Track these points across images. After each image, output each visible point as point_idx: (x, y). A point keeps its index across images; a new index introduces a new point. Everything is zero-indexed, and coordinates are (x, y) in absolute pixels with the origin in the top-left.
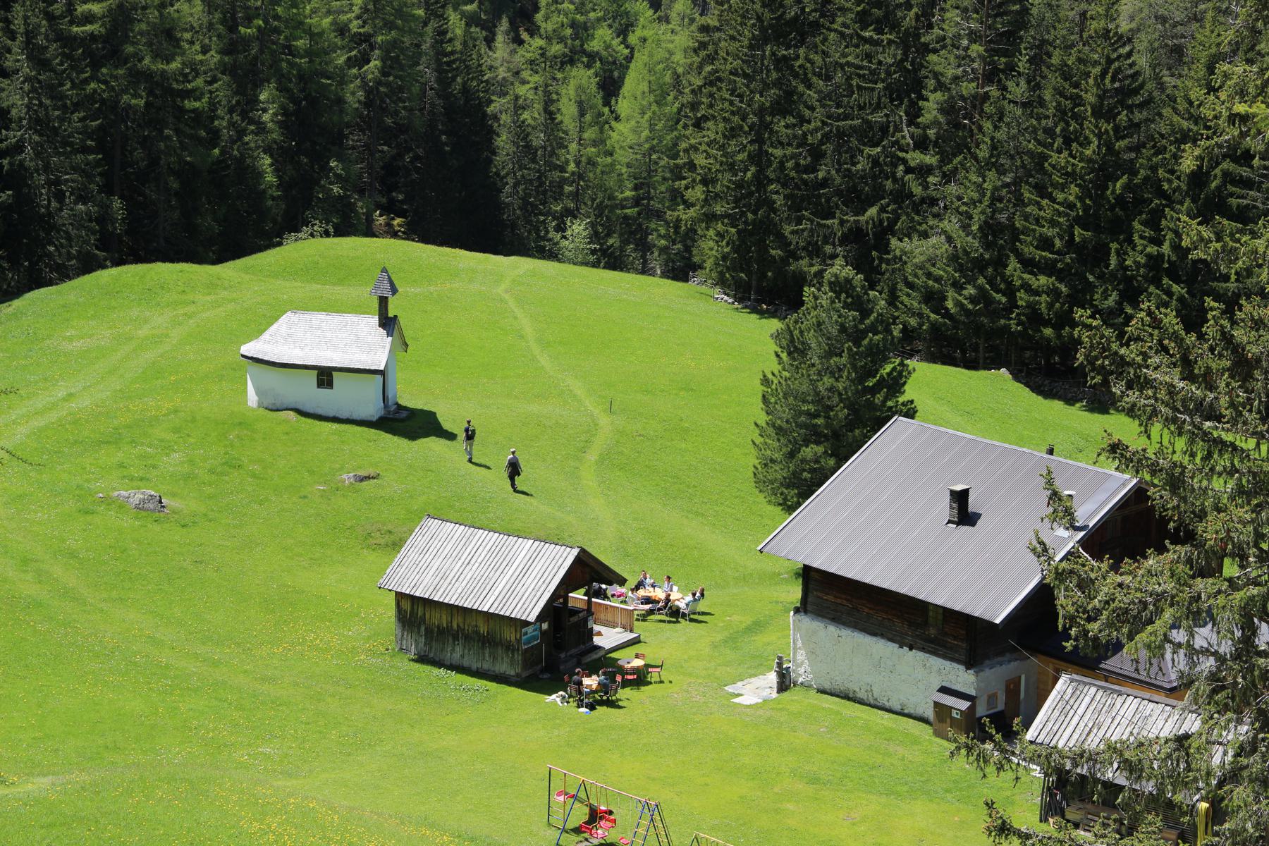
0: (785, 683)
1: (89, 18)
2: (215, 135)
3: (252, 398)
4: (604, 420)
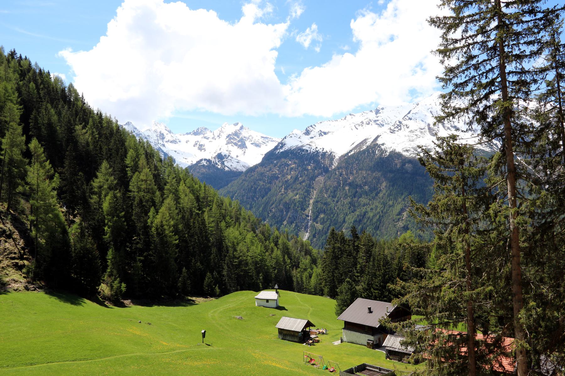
0: (342, 342)
1: (236, 262)
2: (253, 279)
4: (311, 309)
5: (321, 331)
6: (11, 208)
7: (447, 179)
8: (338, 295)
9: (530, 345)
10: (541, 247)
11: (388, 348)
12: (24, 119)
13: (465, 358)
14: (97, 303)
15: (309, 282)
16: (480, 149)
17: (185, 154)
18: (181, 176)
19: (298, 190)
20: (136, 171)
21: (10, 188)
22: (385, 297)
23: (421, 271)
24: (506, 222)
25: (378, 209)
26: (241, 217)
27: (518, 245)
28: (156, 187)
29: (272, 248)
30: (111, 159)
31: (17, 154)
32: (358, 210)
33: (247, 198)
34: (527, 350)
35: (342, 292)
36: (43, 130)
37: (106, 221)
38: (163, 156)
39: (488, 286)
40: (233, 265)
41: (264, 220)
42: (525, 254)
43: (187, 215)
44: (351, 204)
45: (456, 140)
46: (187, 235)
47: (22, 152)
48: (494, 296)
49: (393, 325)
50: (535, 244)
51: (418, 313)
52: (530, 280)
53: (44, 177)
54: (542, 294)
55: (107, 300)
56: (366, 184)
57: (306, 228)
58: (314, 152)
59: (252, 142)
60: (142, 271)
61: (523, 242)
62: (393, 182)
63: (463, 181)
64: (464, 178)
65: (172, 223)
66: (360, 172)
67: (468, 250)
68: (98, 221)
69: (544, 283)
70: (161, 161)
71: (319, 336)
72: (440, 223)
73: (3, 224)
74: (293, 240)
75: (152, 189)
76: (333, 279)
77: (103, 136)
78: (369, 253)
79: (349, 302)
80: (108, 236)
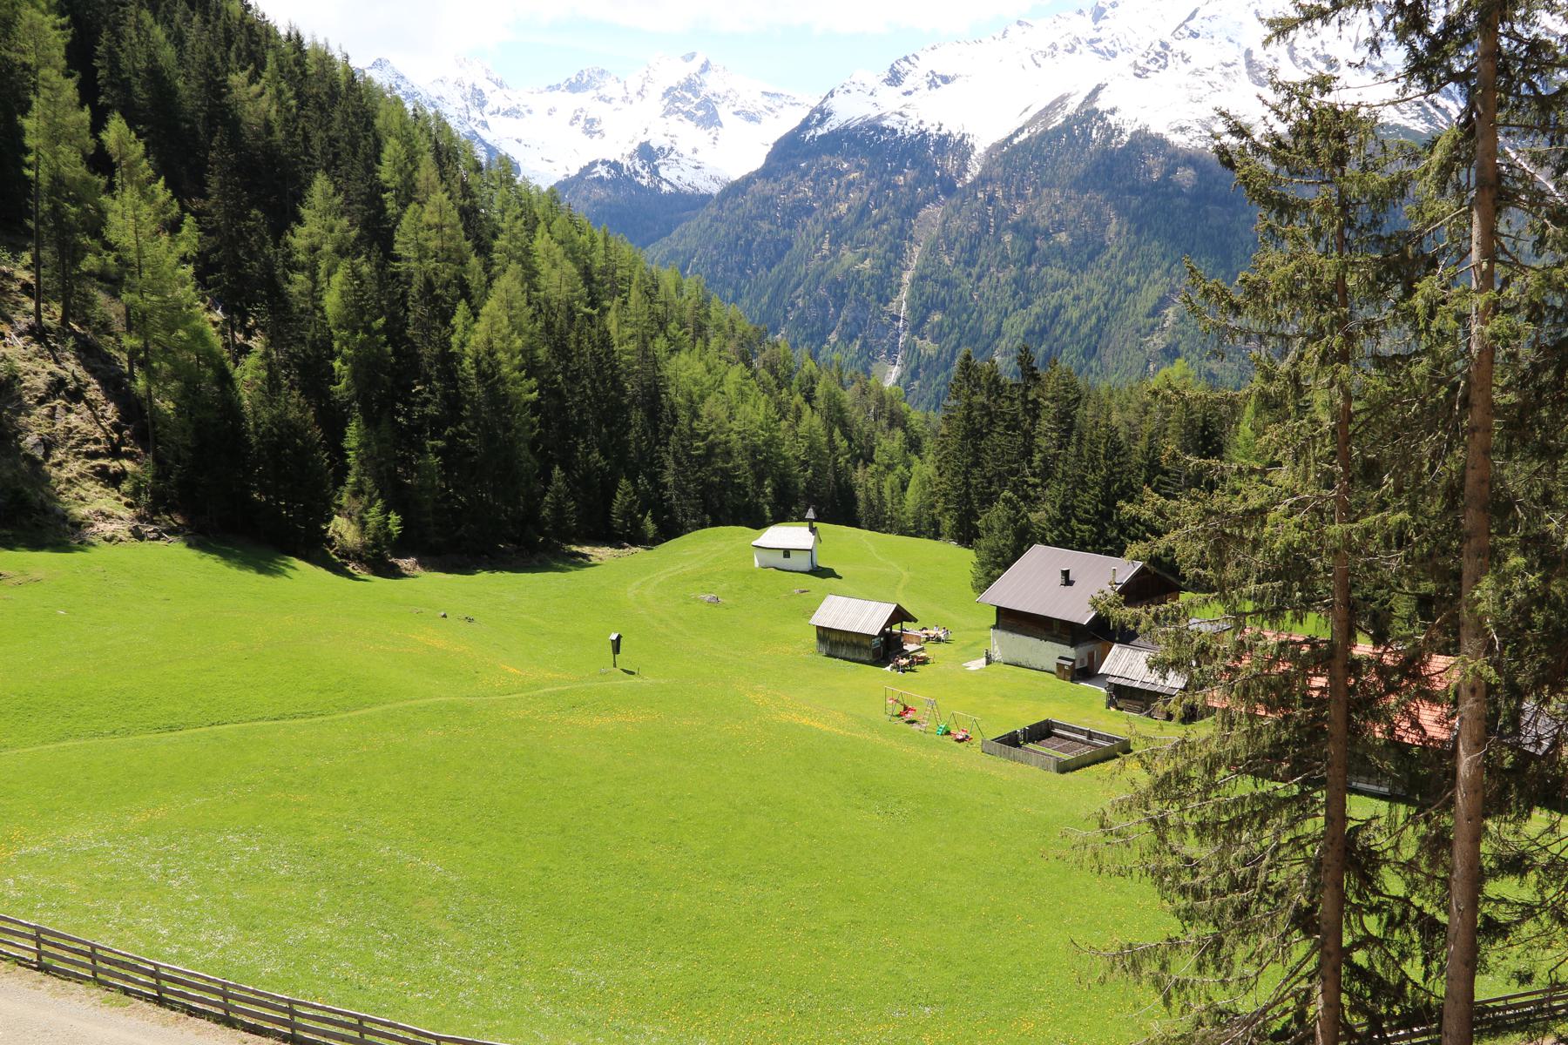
0: (989, 661)
1: (698, 448)
2: (746, 494)
3: (757, 564)
5: (932, 633)
6: (73, 316)
7: (1296, 207)
8: (978, 537)
9: (1499, 673)
10: (1553, 405)
11: (1113, 680)
12: (79, 57)
13: (1320, 702)
14: (328, 568)
15: (900, 502)
16: (1397, 126)
17: (545, 149)
18: (535, 213)
19: (870, 244)
20: (411, 200)
21: (62, 260)
22: (1109, 541)
23: (1210, 467)
24: (1460, 332)
25: (1095, 299)
26: (711, 324)
27: (1489, 398)
28: (469, 244)
29: (798, 408)
30: (337, 167)
31: (73, 167)
32: (1038, 302)
33: (725, 270)
34: (1488, 684)
35: (989, 530)
36: (137, 89)
37: (336, 345)
38: (484, 155)
39: (1395, 512)
40: (689, 456)
41: (776, 331)
42: (1509, 425)
43: (560, 320)
44: (1020, 283)
45: (1329, 90)
46: (560, 377)
47: (85, 156)
48: (1409, 540)
49: (1129, 612)
50: (1538, 396)
51: (1199, 585)
52: (1516, 497)
53: (153, 227)
54: (1545, 536)
55: (353, 560)
56: (1061, 225)
57: (892, 351)
58: (913, 136)
59: (737, 109)
60: (442, 478)
61: (1504, 390)
62: (1140, 223)
63: (1340, 214)
64: (1345, 205)
65: (519, 343)
66: (1045, 191)
67: (1346, 410)
68: (313, 345)
69: (1555, 507)
70: (478, 168)
71: (928, 646)
72: (1270, 334)
73: (57, 362)
74: (856, 385)
75: (458, 250)
76: (967, 494)
77: (311, 102)
78: (1066, 423)
79: (1009, 554)
80: (342, 386)
